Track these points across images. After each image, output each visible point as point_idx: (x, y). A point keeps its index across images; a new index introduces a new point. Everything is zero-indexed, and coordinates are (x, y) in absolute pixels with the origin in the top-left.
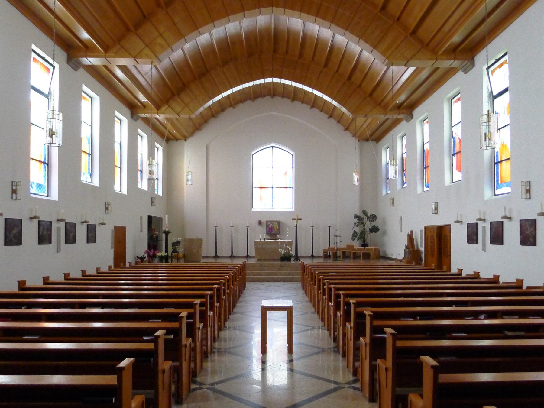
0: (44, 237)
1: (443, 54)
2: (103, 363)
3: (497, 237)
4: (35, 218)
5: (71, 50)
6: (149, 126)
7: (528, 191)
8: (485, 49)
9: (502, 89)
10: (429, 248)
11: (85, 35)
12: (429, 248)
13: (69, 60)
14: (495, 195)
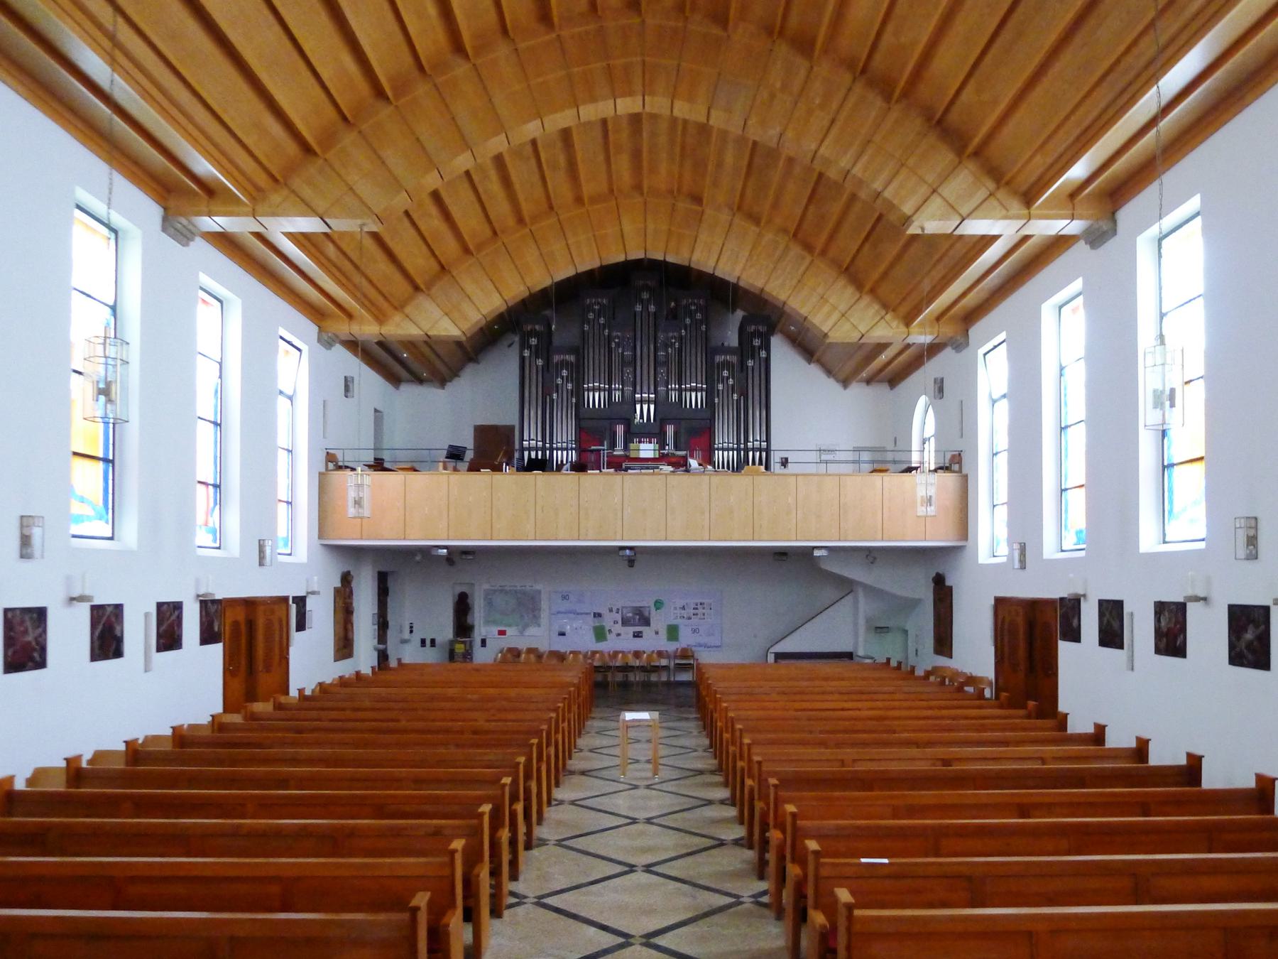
0: (106, 638)
1: (922, 324)
2: (271, 860)
3: (1171, 640)
4: (81, 599)
5: (176, 193)
6: (356, 355)
7: (1252, 541)
8: (1156, 184)
9: (838, 649)
10: (1006, 650)
11: (203, 166)
12: (1006, 650)
13: (168, 223)
14: (1165, 542)
